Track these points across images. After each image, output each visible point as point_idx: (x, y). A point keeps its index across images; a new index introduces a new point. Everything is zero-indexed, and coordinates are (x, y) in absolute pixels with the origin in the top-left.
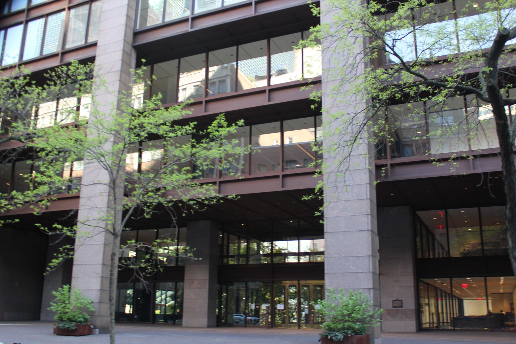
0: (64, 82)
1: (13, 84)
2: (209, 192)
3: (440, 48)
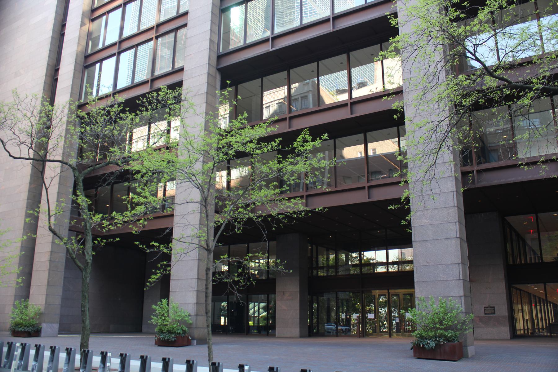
0: (155, 107)
1: (109, 112)
2: (297, 206)
3: (524, 50)
